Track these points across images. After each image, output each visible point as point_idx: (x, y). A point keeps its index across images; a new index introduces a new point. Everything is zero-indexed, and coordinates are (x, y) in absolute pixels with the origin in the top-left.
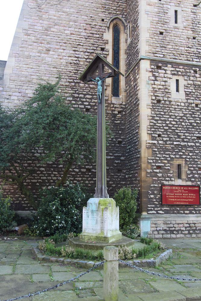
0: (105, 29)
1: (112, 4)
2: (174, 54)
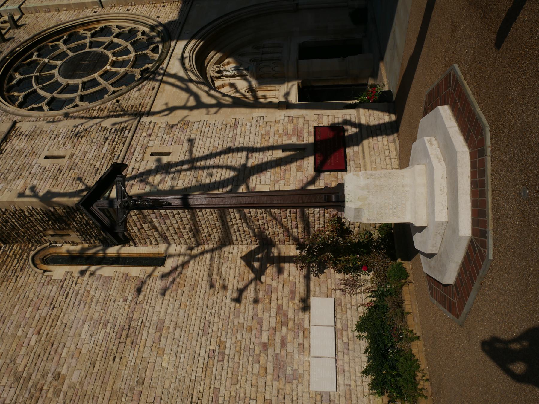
0: (46, 277)
1: (7, 266)
2: (110, 159)
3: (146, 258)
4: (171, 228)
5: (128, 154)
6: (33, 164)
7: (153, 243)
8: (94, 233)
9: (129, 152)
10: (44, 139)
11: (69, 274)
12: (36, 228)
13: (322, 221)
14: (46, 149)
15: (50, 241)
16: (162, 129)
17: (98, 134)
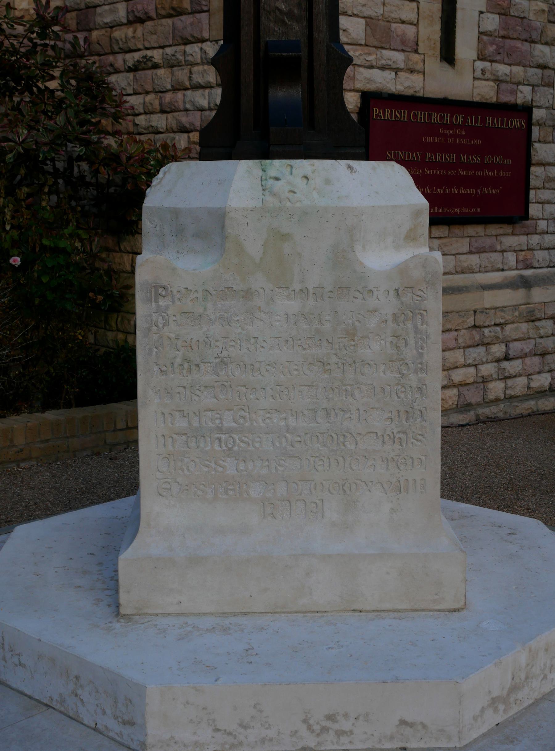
13: (159, 121)
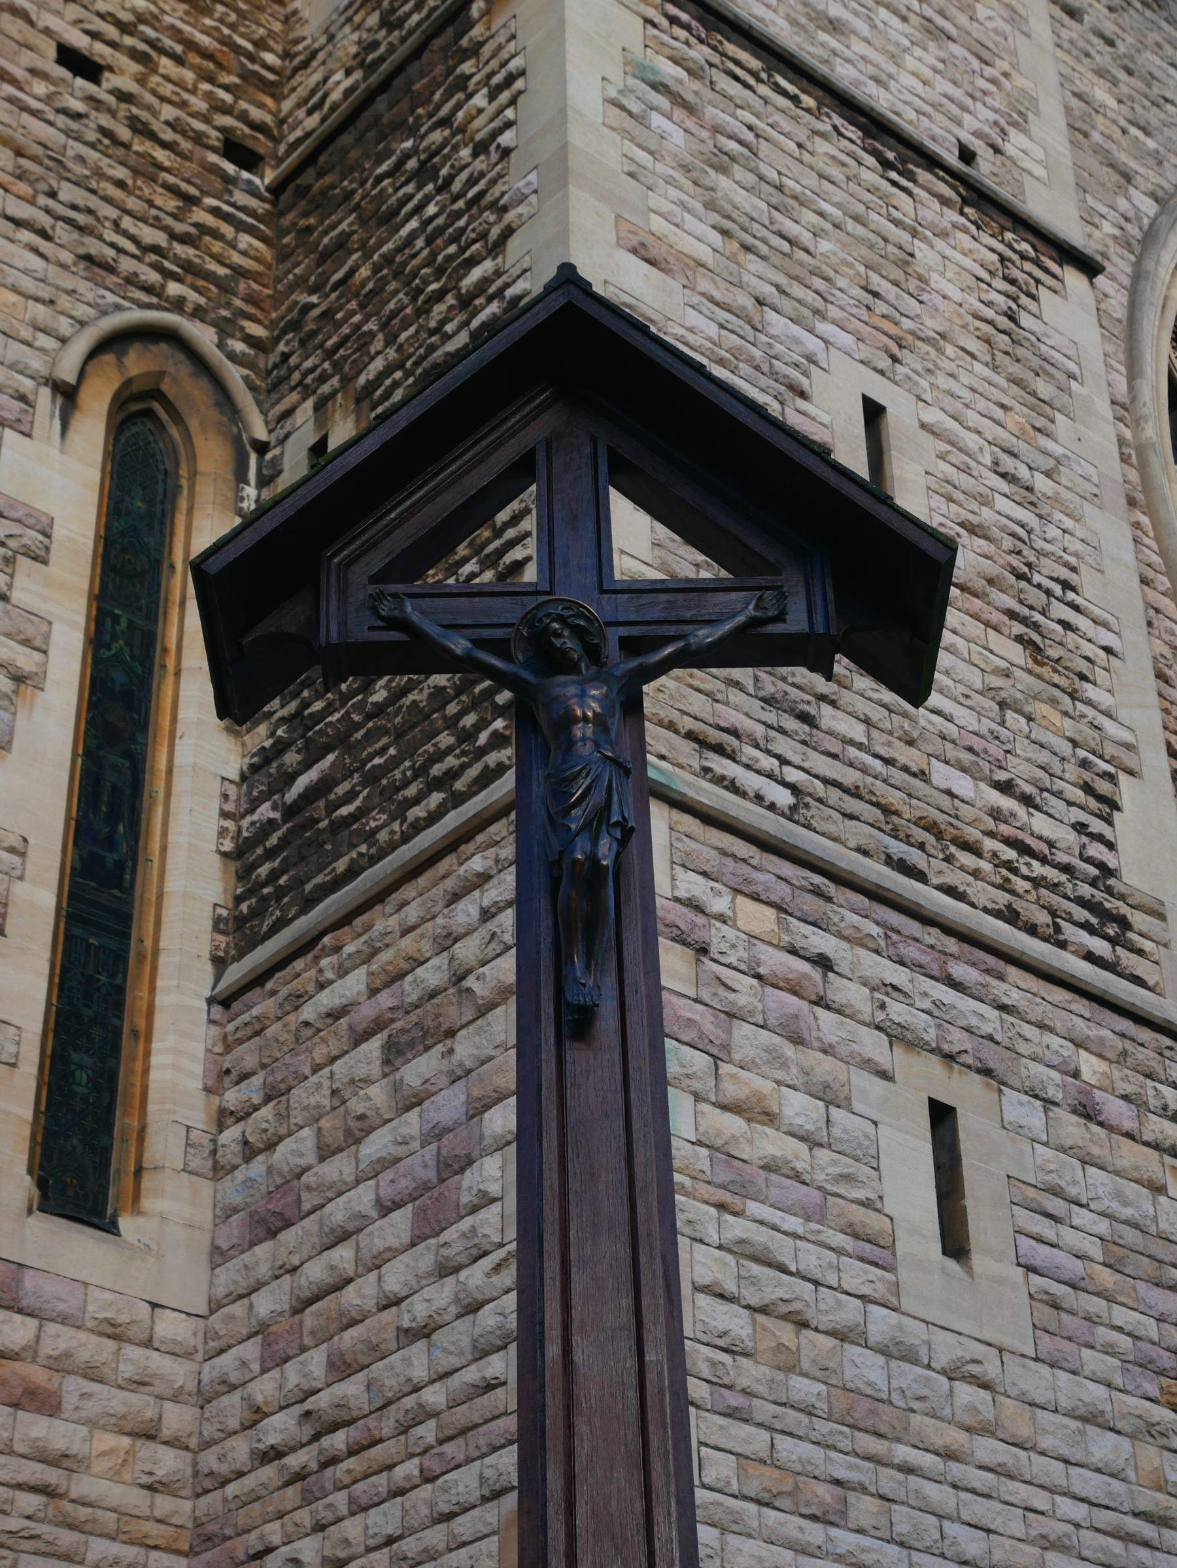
0: (22, 398)
1: (120, 184)
2: (887, 810)
3: (113, 1076)
4: (343, 1255)
5: (932, 936)
6: (823, 327)
7: (230, 1135)
8: (329, 709)
9: (952, 945)
10: (999, 413)
11: (32, 537)
12: (378, 344)
14: (932, 416)
15: (282, 442)
16: (1143, 1203)
17: (1066, 748)
